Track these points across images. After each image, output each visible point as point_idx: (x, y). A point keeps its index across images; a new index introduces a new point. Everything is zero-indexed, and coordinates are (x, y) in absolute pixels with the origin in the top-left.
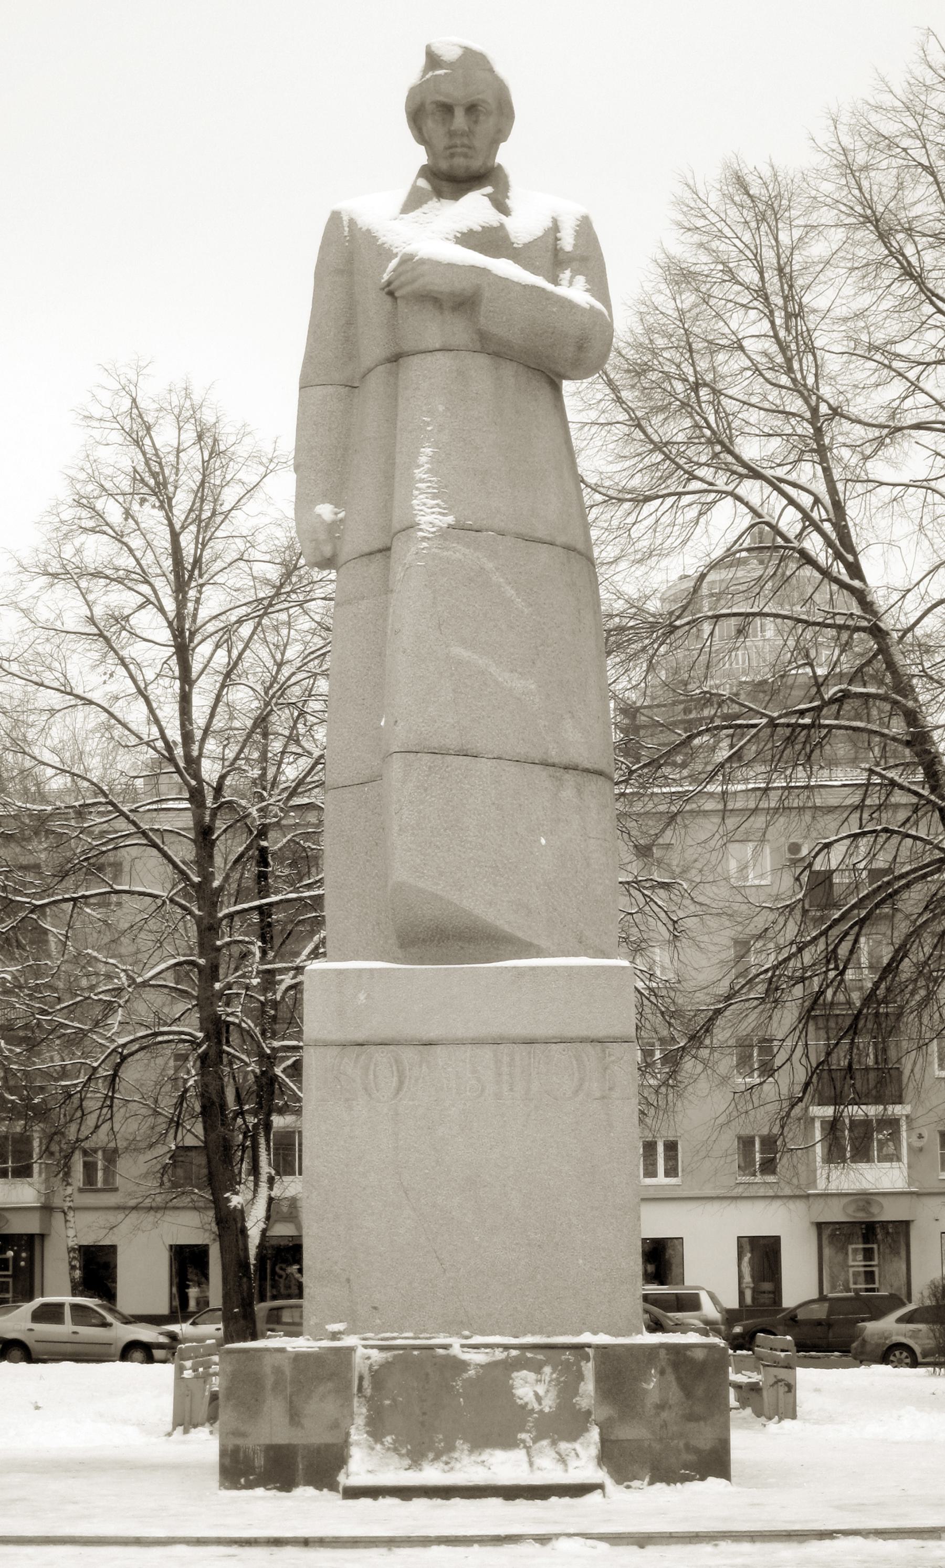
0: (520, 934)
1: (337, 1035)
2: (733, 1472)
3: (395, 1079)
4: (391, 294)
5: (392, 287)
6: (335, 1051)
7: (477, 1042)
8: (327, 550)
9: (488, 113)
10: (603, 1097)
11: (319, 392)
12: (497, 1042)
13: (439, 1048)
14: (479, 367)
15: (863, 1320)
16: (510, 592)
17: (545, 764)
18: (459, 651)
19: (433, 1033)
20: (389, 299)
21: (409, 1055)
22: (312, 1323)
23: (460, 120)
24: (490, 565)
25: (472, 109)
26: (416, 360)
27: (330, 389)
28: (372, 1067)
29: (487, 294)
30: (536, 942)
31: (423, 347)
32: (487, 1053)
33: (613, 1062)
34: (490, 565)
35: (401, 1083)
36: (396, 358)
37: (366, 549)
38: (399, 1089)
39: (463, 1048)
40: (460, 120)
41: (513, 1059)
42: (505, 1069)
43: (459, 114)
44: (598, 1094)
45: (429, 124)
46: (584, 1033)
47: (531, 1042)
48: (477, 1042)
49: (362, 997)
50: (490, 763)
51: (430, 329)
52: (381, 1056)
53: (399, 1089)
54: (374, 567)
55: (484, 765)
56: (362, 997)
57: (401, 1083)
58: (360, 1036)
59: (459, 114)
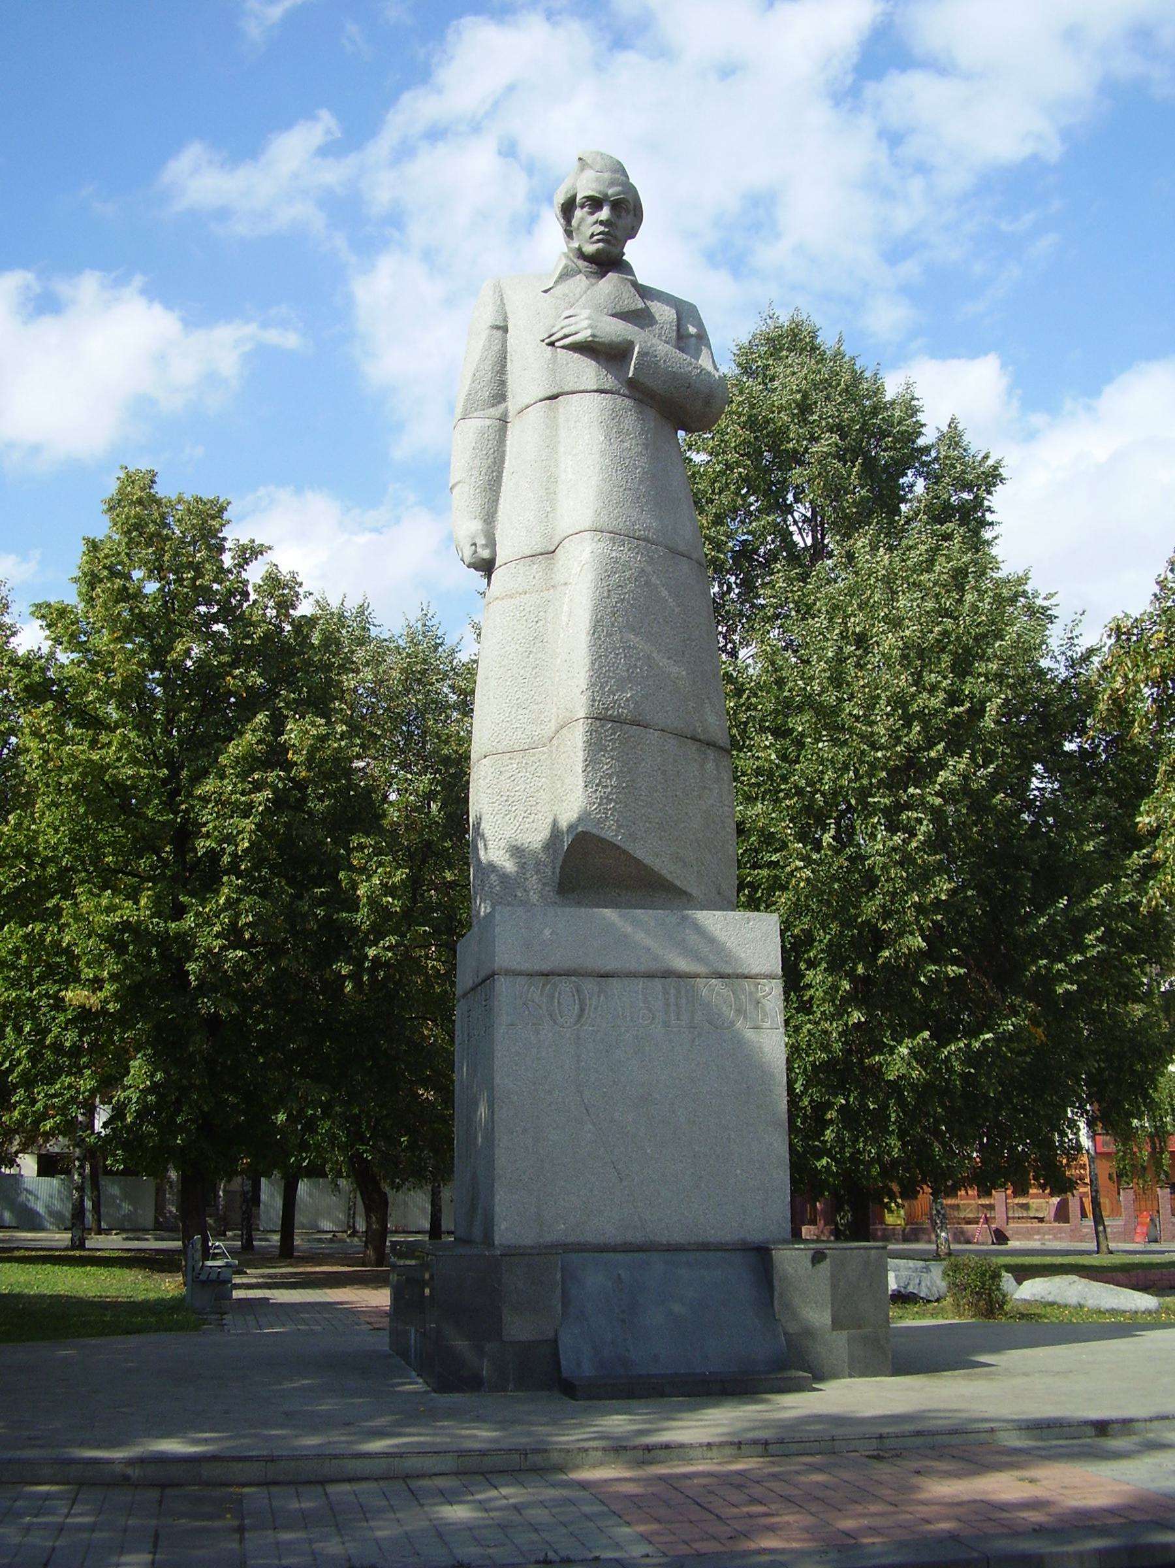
0: (678, 883)
1: (526, 966)
3: (577, 1006)
8: (485, 554)
9: (628, 212)
15: (436, 1505)
16: (665, 593)
17: (694, 739)
19: (611, 965)
21: (589, 985)
22: (503, 1227)
28: (557, 995)
30: (689, 891)
33: (764, 997)
35: (582, 1010)
38: (580, 1016)
39: (636, 980)
41: (679, 992)
42: (672, 1000)
49: (547, 932)
50: (657, 733)
52: (566, 986)
53: (580, 1016)
54: (537, 568)
55: (653, 736)
56: (547, 932)
57: (582, 1010)
58: (546, 967)
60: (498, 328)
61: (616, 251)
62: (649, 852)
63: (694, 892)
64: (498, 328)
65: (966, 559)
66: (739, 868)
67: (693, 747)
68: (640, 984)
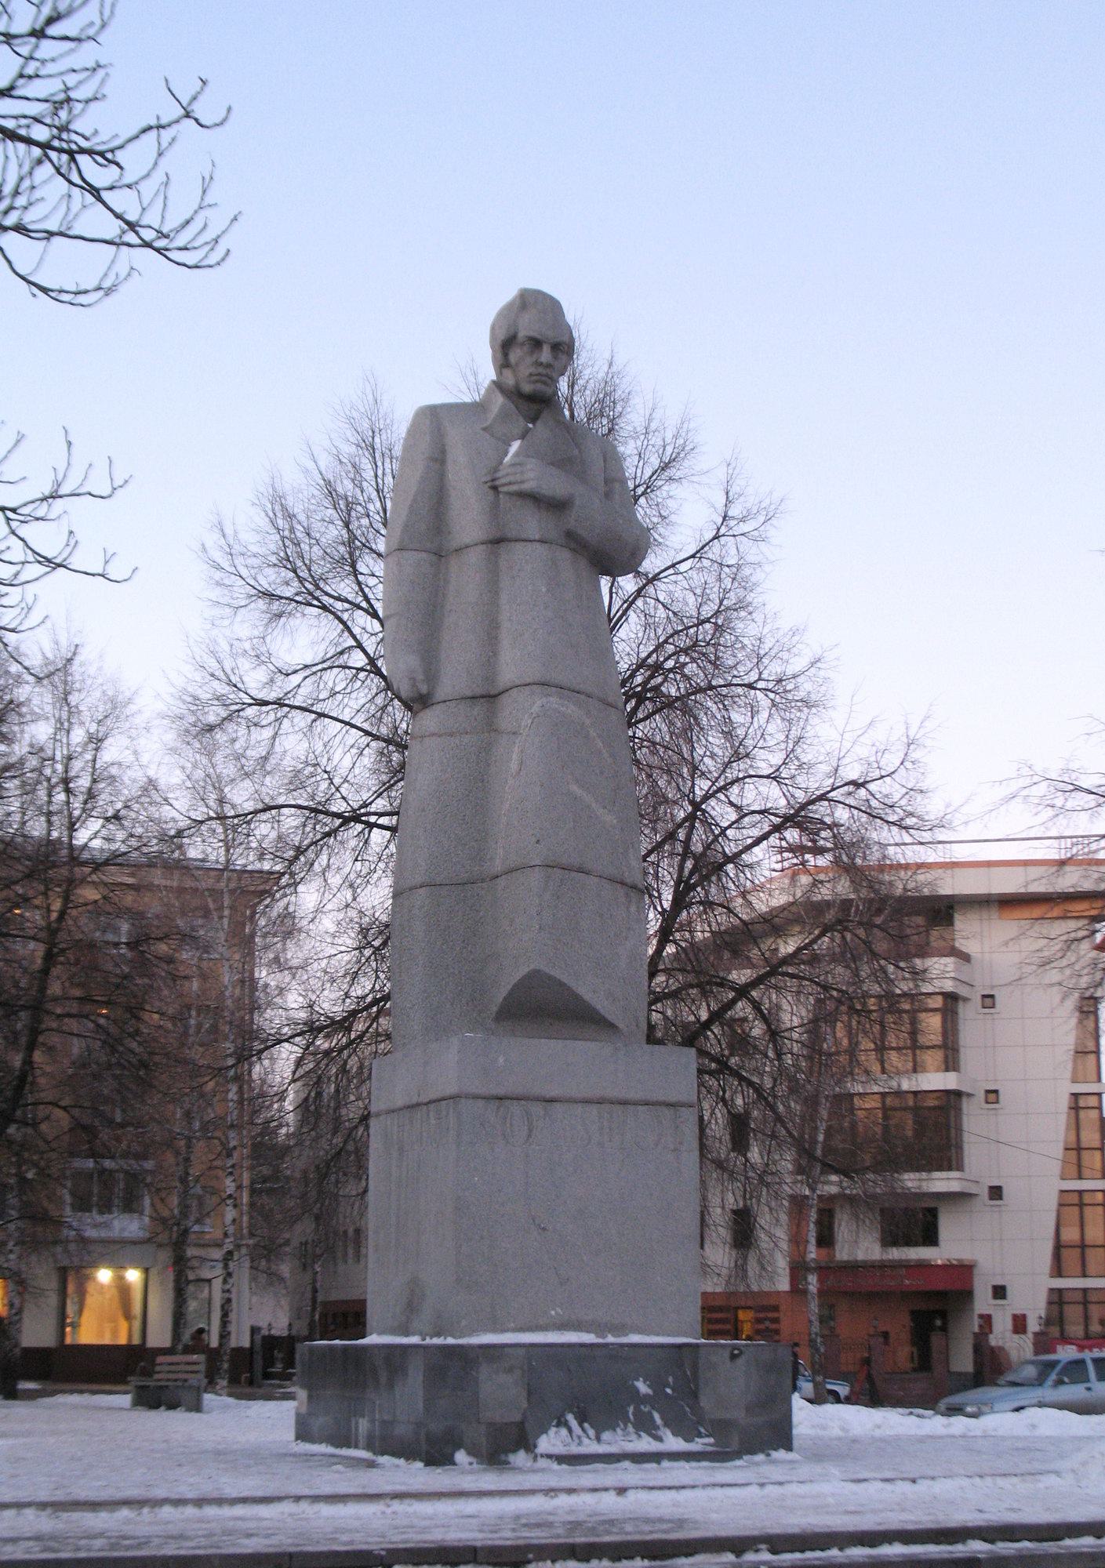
2: (796, 1443)
4: (495, 488)
5: (497, 483)
6: (481, 1103)
7: (587, 1101)
10: (675, 1150)
11: (412, 557)
12: (600, 1101)
13: (558, 1105)
14: (564, 556)
17: (622, 883)
18: (574, 788)
19: (554, 1092)
20: (491, 492)
21: (537, 1109)
23: (546, 355)
24: (588, 722)
25: (556, 347)
26: (519, 546)
27: (424, 555)
29: (577, 502)
31: (524, 536)
32: (594, 1110)
34: (588, 722)
35: (530, 1131)
36: (497, 542)
37: (469, 693)
38: (529, 1136)
40: (546, 355)
43: (546, 349)
44: (672, 1147)
45: (515, 355)
46: (662, 1098)
47: (624, 1103)
48: (587, 1101)
49: (501, 1060)
51: (532, 523)
52: (516, 1108)
53: (529, 1136)
54: (478, 710)
56: (501, 1060)
57: (530, 1131)
58: (501, 1091)
59: (546, 349)
60: (436, 460)
61: (549, 391)
62: (591, 990)
63: (621, 1026)
64: (436, 460)
65: (796, 1048)
66: (1058, 1270)
67: (621, 891)
68: (579, 1109)
